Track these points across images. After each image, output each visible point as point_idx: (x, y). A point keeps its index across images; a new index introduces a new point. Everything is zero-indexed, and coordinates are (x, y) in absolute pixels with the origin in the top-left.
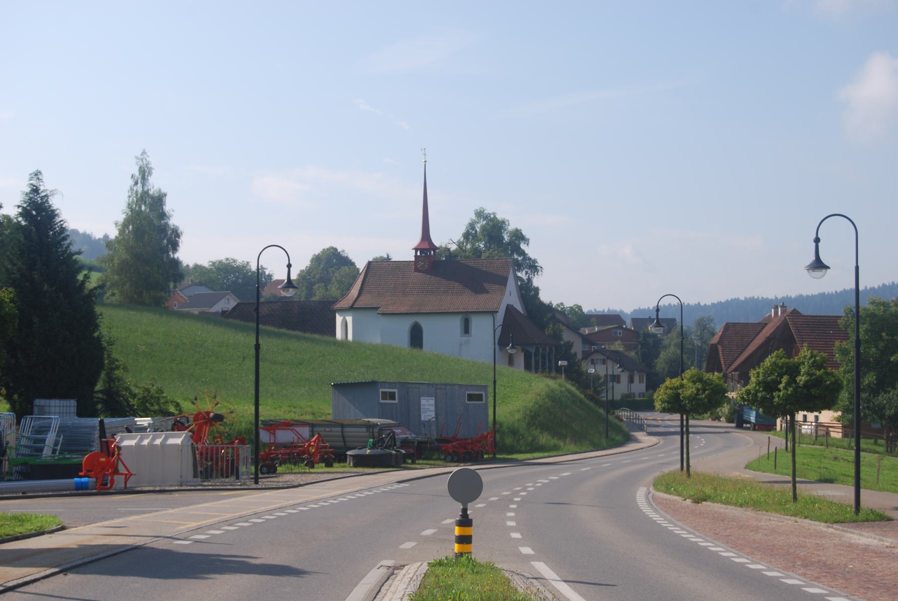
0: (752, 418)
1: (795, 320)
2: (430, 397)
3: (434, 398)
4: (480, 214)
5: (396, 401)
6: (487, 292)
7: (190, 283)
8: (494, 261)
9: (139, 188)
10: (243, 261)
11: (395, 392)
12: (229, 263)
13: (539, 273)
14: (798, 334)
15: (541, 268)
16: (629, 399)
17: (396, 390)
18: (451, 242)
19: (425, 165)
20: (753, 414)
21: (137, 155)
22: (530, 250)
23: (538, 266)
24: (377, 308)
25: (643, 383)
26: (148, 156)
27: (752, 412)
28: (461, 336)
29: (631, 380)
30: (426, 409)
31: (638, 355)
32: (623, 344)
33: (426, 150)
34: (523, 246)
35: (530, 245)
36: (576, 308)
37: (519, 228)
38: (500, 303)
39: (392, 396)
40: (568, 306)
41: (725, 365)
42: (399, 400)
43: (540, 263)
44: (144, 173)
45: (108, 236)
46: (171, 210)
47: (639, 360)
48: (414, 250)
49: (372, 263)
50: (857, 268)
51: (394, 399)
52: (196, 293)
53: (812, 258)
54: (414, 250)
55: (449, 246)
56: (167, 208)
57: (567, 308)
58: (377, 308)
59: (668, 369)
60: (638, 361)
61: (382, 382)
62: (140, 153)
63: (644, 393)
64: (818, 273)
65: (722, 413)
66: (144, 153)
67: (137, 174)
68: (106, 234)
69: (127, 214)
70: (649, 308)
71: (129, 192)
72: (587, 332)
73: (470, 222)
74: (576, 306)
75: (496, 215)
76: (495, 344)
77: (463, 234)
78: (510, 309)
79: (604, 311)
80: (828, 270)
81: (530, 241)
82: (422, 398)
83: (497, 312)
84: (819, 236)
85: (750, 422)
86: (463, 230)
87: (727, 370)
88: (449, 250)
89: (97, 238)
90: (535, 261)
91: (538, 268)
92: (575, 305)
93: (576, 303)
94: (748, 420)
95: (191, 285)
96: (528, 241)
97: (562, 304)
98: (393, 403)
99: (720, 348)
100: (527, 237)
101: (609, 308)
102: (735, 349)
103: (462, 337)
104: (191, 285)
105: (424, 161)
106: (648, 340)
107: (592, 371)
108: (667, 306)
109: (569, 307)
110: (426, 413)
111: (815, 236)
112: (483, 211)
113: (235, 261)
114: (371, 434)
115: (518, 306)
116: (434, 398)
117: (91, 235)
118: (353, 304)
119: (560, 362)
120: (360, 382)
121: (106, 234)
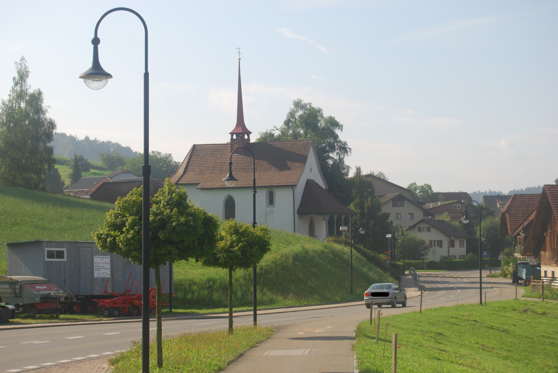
0: (523, 275)
1: (552, 189)
2: (105, 255)
3: (109, 257)
4: (298, 104)
5: (65, 259)
6: (290, 169)
7: (120, 171)
8: (297, 142)
9: (18, 88)
10: (166, 154)
11: (63, 252)
12: (155, 155)
13: (348, 154)
14: (554, 201)
15: (350, 149)
16: (447, 260)
17: (64, 250)
18: (275, 129)
19: (239, 61)
20: (524, 271)
21: (16, 61)
22: (342, 136)
23: (347, 148)
24: (197, 184)
25: (464, 247)
26: (26, 62)
27: (523, 270)
28: (267, 207)
29: (452, 244)
30: (100, 267)
31: (461, 224)
32: (450, 216)
33: (240, 50)
34: (337, 131)
35: (343, 130)
36: (426, 187)
37: (333, 116)
38: (299, 178)
39: (60, 255)
40: (420, 186)
41: (511, 230)
42: (67, 259)
43: (349, 145)
44: (23, 76)
45: (89, 138)
46: (48, 106)
47: (462, 228)
48: (230, 135)
49: (197, 146)
50: (146, 75)
51: (63, 257)
52: (121, 179)
53: (89, 64)
54: (230, 135)
55: (273, 132)
56: (45, 104)
57: (419, 187)
58: (197, 184)
59: (486, 235)
60: (460, 229)
61: (47, 242)
62: (20, 60)
63: (464, 256)
64: (95, 84)
65: (508, 271)
66: (23, 59)
67: (17, 76)
68: (87, 136)
69: (3, 109)
70: (522, 189)
71: (11, 92)
72: (431, 207)
73: (291, 111)
74: (426, 185)
75: (311, 105)
76: (294, 213)
77: (284, 122)
78: (310, 184)
79: (486, 192)
80: (109, 80)
81: (343, 127)
82: (95, 256)
83: (296, 186)
84: (98, 36)
85: (522, 279)
86: (284, 118)
87: (512, 234)
88: (273, 135)
89: (80, 140)
90: (345, 144)
91: (347, 149)
92: (425, 185)
93: (426, 183)
94: (521, 276)
95: (120, 173)
96: (342, 127)
97: (415, 184)
98: (61, 261)
99: (507, 216)
100: (341, 123)
101: (490, 190)
102: (520, 217)
103: (267, 207)
104: (120, 173)
105: (238, 58)
106: (482, 212)
107: (389, 236)
108: (536, 188)
109: (421, 186)
110: (100, 270)
111: (93, 36)
112: (300, 103)
113: (159, 153)
114: (13, 290)
115: (320, 181)
116: (109, 257)
117: (76, 137)
118: (178, 181)
119: (341, 228)
120: (18, 242)
121: (87, 136)
